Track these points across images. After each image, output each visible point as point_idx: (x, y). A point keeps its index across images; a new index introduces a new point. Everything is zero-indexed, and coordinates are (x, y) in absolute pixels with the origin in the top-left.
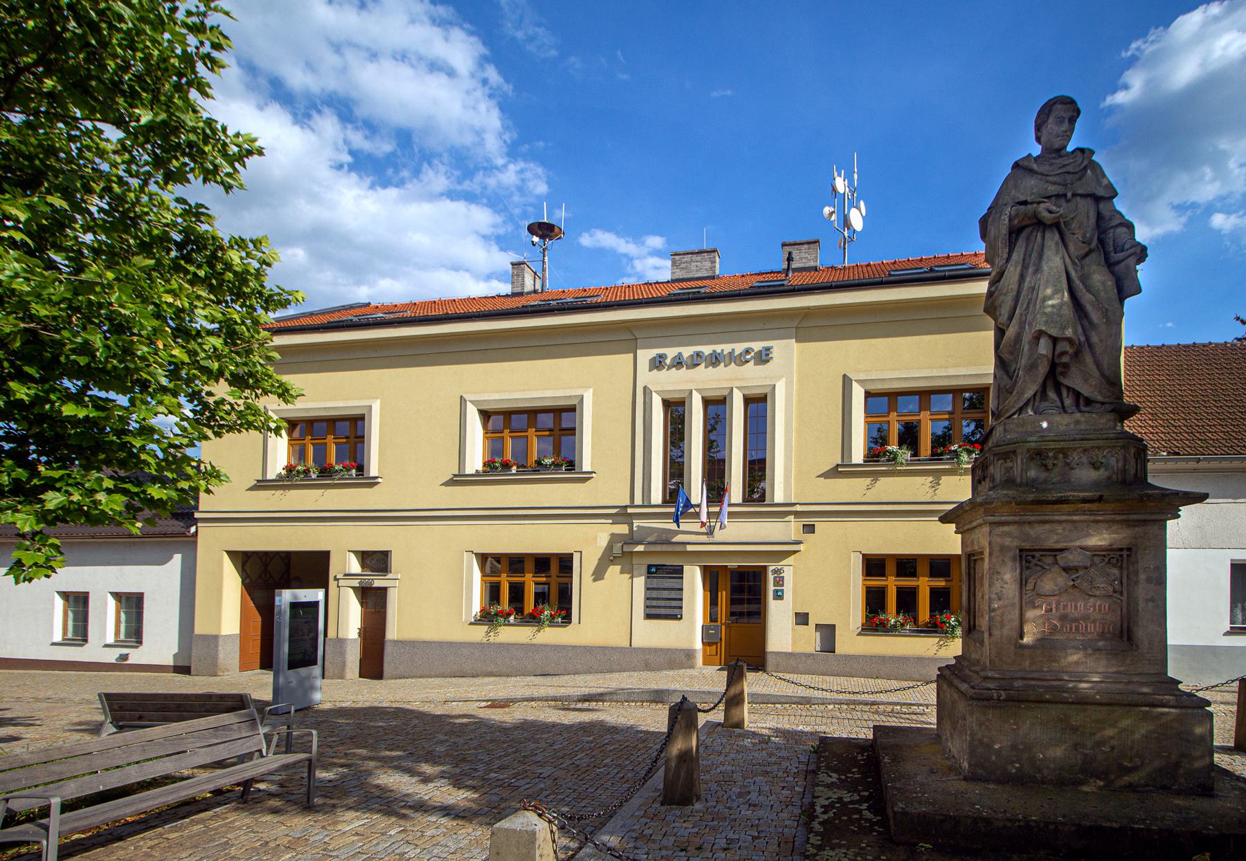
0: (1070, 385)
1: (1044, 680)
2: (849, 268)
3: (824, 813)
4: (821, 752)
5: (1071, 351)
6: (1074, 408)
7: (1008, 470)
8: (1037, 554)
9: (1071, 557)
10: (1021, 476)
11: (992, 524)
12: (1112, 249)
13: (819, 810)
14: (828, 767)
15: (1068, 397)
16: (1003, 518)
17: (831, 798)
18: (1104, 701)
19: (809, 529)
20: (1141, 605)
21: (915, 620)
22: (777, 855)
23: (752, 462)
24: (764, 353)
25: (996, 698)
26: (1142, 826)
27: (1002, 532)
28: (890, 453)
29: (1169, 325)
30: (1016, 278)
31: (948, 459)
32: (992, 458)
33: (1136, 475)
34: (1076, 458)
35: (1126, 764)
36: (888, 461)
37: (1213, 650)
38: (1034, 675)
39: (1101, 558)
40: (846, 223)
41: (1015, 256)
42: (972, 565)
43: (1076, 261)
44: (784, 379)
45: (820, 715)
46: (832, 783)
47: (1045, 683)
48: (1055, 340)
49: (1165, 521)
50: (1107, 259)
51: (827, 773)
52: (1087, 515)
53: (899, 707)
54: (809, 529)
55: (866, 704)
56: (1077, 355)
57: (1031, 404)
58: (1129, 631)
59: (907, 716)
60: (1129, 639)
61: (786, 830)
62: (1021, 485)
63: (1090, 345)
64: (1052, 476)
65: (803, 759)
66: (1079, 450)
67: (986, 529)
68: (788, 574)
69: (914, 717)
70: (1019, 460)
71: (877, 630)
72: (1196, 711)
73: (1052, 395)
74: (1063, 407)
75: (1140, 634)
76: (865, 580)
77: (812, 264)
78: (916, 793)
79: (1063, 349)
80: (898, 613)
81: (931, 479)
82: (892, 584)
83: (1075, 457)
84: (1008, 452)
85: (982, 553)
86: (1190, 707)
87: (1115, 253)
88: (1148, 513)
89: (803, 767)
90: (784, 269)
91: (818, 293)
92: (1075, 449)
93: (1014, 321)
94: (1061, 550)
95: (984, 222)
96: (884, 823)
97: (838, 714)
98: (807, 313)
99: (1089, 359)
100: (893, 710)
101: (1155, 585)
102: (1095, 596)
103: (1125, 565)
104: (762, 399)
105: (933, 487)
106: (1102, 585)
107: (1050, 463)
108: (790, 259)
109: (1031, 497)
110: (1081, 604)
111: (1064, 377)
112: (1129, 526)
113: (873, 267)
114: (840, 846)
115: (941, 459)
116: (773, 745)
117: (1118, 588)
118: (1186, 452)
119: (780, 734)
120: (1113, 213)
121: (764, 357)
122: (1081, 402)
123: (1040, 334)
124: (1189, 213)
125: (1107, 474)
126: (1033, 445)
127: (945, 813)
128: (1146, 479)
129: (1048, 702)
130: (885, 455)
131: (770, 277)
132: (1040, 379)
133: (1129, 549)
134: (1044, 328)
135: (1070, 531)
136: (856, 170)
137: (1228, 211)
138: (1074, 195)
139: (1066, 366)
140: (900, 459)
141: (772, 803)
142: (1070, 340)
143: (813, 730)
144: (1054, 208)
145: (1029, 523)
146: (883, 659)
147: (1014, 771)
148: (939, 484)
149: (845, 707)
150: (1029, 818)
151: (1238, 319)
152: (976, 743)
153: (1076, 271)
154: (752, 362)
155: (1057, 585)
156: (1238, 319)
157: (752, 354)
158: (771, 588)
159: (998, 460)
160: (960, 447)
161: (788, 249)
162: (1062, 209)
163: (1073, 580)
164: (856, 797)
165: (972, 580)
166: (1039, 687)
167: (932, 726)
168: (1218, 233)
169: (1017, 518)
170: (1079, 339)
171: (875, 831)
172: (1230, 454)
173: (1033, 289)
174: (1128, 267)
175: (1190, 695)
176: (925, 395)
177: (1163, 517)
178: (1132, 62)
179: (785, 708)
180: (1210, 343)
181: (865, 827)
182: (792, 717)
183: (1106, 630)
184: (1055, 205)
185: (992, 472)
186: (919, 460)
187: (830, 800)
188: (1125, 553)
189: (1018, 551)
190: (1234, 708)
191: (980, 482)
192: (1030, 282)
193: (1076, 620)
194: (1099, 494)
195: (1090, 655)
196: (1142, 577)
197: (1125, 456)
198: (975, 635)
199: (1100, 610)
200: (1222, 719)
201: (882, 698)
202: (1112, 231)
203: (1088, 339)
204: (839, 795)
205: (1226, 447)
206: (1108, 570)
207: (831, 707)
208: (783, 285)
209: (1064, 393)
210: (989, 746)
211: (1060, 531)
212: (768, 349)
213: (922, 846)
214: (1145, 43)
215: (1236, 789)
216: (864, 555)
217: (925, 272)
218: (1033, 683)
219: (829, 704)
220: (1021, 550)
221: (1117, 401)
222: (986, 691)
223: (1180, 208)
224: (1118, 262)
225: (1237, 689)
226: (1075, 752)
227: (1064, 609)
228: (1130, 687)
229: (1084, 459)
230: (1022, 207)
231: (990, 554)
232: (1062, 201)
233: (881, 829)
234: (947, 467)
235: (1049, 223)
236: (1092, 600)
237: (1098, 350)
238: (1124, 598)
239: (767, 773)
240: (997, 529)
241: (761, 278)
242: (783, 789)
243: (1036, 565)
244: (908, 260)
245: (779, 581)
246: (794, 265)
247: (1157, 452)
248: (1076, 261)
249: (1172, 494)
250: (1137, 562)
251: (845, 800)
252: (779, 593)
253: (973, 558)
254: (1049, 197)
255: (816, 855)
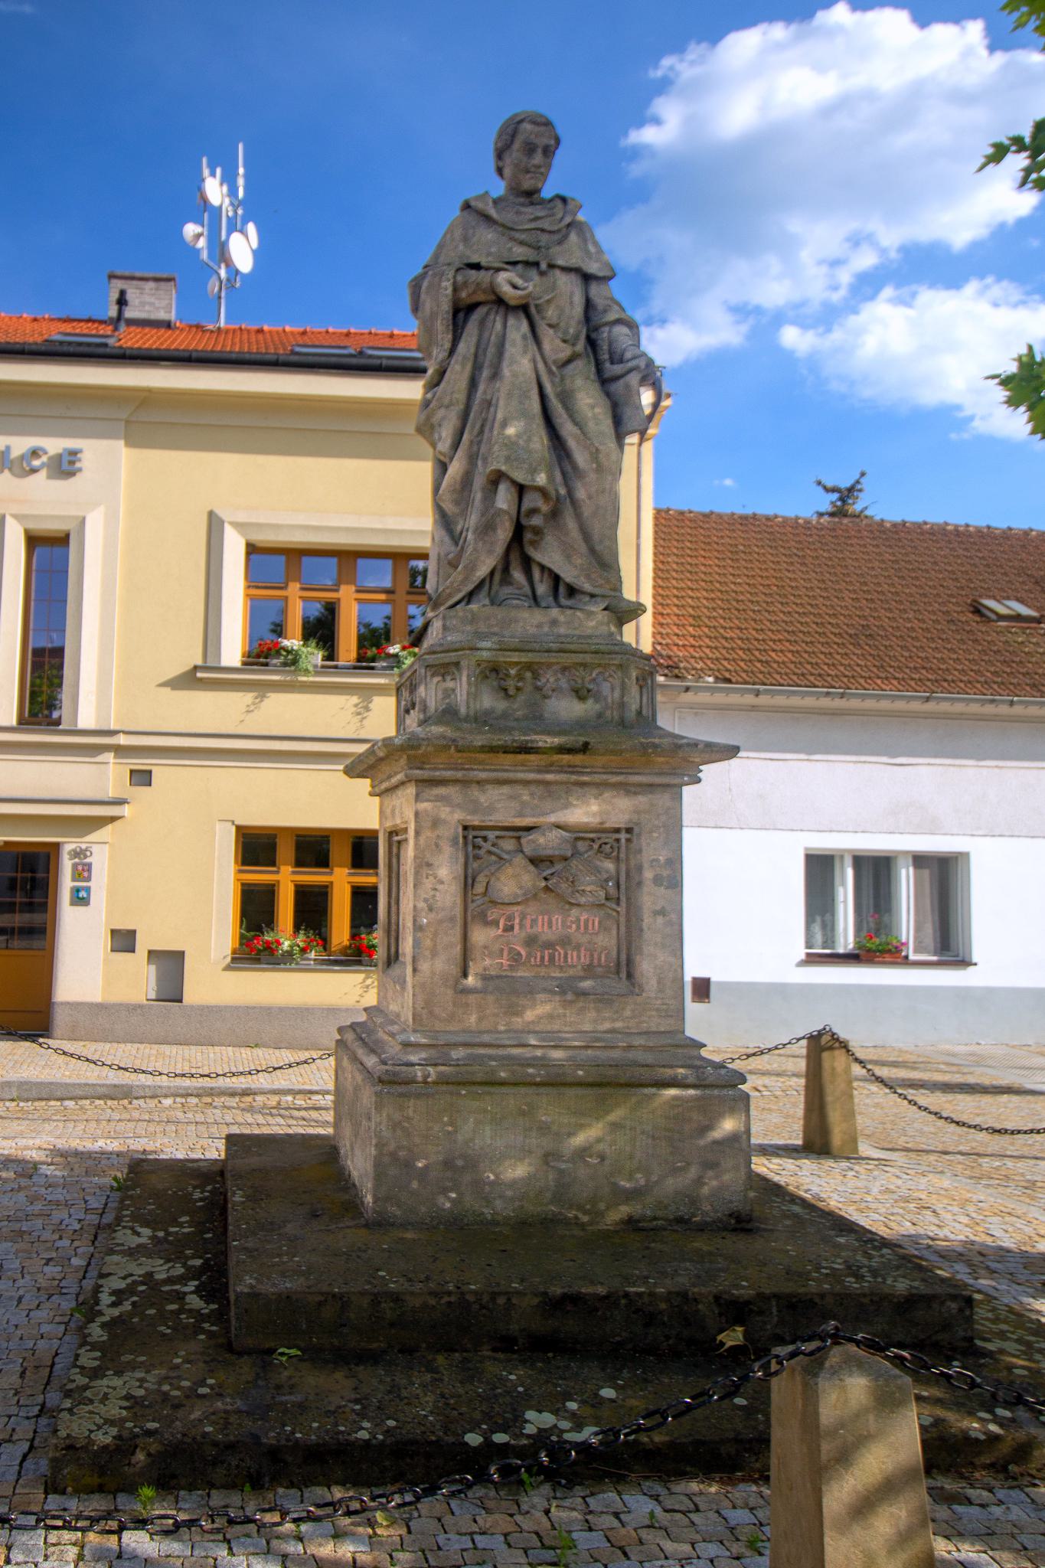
0: (546, 562)
1: (499, 1046)
2: (227, 332)
3: (114, 1305)
4: (128, 1188)
5: (545, 508)
6: (551, 598)
7: (448, 693)
8: (491, 835)
9: (542, 840)
10: (468, 703)
11: (420, 782)
12: (606, 356)
13: (106, 1299)
14: (134, 1218)
15: (542, 581)
16: (438, 773)
17: (132, 1275)
18: (590, 1080)
19: (143, 778)
20: (647, 920)
21: (325, 942)
22: (15, 1394)
23: (38, 653)
24: (66, 459)
25: (420, 1079)
26: (643, 1290)
27: (437, 796)
28: (289, 652)
29: (728, 482)
30: (463, 384)
31: (384, 668)
32: (423, 671)
33: (639, 713)
34: (552, 680)
35: (622, 1183)
36: (285, 664)
37: (780, 990)
38: (486, 1038)
39: (587, 843)
40: (221, 252)
41: (462, 347)
42: (395, 850)
43: (554, 368)
44: (102, 509)
45: (147, 1117)
46: (139, 1246)
47: (501, 1052)
48: (521, 489)
49: (680, 786)
50: (599, 370)
51: (132, 1229)
52: (566, 772)
53: (290, 1098)
54: (143, 778)
55: (233, 1094)
56: (555, 514)
57: (486, 588)
58: (630, 962)
59: (303, 1113)
60: (630, 976)
61: (41, 1344)
62: (467, 719)
63: (574, 502)
64: (515, 706)
65: (95, 1203)
66: (555, 667)
67: (411, 790)
68: (100, 860)
69: (314, 1114)
70: (464, 679)
71: (258, 961)
72: (725, 1092)
73: (518, 575)
74: (535, 597)
75: (647, 968)
76: (240, 871)
77: (162, 315)
78: (279, 1256)
79: (532, 505)
80: (297, 928)
81: (355, 699)
82: (286, 879)
83: (549, 679)
84: (448, 664)
85: (405, 830)
86: (717, 1086)
87: (612, 363)
88: (656, 774)
89: (93, 1219)
90: (111, 319)
91: (166, 367)
92: (549, 665)
93: (460, 453)
94: (529, 829)
95: (416, 286)
96: (220, 1316)
97: (180, 1115)
98: (146, 398)
99: (571, 524)
100: (279, 1103)
101: (667, 888)
102: (578, 905)
103: (622, 855)
104: (61, 541)
105: (359, 714)
106: (588, 889)
107: (511, 684)
108: (122, 302)
109: (479, 741)
110: (557, 918)
111: (535, 549)
112: (628, 793)
113: (268, 336)
114: (133, 1366)
115: (372, 668)
116: (42, 1181)
117: (613, 892)
118: (740, 680)
119: (57, 1159)
120: (609, 302)
121: (65, 466)
122: (562, 589)
123: (497, 478)
124: (751, 321)
125: (598, 707)
126: (485, 654)
127: (325, 1289)
128: (654, 719)
129: (503, 1083)
130: (278, 654)
131: (84, 328)
132: (500, 549)
133: (629, 830)
134: (503, 468)
135: (541, 798)
136: (241, 171)
137: (804, 324)
138: (551, 266)
139: (537, 531)
140: (303, 663)
141: (21, 1292)
142: (542, 491)
143: (124, 1149)
144: (519, 282)
145: (478, 782)
146: (267, 1012)
147: (448, 1205)
148: (367, 709)
149: (194, 1100)
150: (464, 1288)
151: (819, 483)
152: (386, 1159)
153: (552, 382)
154: (43, 473)
155: (521, 888)
156: (819, 483)
157: (44, 459)
158: (66, 883)
159: (433, 675)
160: (404, 648)
161: (118, 285)
162: (532, 285)
163: (546, 879)
164: (179, 1270)
165: (394, 875)
166: (491, 1058)
167: (321, 1131)
168: (787, 357)
169: (459, 775)
170: (557, 491)
171: (204, 1331)
172: (800, 686)
173: (489, 404)
174: (627, 386)
175: (721, 1066)
176: (348, 559)
177: (676, 781)
178: (664, 86)
179: (82, 1108)
180: (776, 516)
181: (186, 1327)
182: (93, 1124)
183: (596, 961)
184: (521, 276)
185: (423, 695)
186: (336, 667)
187: (129, 1280)
188: (623, 836)
189: (460, 829)
190: (802, 1081)
191: (407, 711)
192: (485, 392)
193: (549, 945)
194: (582, 739)
195: (571, 1002)
196: (648, 874)
197: (623, 681)
198: (396, 970)
199: (586, 927)
200: (793, 1100)
201: (263, 1081)
202: (607, 329)
203: (570, 493)
204: (149, 1269)
205: (795, 674)
206: (598, 863)
207: (168, 1102)
208: (106, 345)
209: (536, 573)
210: (408, 1164)
211: (526, 798)
212: (74, 453)
213: (283, 1354)
214: (682, 61)
215: (787, 1217)
216: (239, 828)
217: (351, 356)
218: (482, 1051)
219: (166, 1096)
220: (465, 828)
221: (613, 593)
222: (404, 1068)
223: (741, 311)
224: (616, 378)
225: (804, 1051)
226: (545, 1167)
227: (532, 927)
228: (631, 1055)
229: (564, 683)
230: (473, 272)
231: (417, 833)
232: (533, 273)
233: (214, 1328)
234: (382, 681)
235: (513, 303)
236: (575, 912)
237: (587, 511)
238: (622, 909)
239: (21, 1233)
240: (427, 790)
241: (68, 328)
242: (47, 1264)
243: (490, 852)
244: (327, 332)
245: (83, 872)
246: (129, 313)
247: (700, 677)
248: (554, 368)
249: (688, 745)
250: (640, 851)
251: (158, 1277)
252: (83, 894)
253: (396, 838)
254: (514, 263)
255: (86, 1388)
